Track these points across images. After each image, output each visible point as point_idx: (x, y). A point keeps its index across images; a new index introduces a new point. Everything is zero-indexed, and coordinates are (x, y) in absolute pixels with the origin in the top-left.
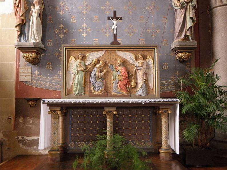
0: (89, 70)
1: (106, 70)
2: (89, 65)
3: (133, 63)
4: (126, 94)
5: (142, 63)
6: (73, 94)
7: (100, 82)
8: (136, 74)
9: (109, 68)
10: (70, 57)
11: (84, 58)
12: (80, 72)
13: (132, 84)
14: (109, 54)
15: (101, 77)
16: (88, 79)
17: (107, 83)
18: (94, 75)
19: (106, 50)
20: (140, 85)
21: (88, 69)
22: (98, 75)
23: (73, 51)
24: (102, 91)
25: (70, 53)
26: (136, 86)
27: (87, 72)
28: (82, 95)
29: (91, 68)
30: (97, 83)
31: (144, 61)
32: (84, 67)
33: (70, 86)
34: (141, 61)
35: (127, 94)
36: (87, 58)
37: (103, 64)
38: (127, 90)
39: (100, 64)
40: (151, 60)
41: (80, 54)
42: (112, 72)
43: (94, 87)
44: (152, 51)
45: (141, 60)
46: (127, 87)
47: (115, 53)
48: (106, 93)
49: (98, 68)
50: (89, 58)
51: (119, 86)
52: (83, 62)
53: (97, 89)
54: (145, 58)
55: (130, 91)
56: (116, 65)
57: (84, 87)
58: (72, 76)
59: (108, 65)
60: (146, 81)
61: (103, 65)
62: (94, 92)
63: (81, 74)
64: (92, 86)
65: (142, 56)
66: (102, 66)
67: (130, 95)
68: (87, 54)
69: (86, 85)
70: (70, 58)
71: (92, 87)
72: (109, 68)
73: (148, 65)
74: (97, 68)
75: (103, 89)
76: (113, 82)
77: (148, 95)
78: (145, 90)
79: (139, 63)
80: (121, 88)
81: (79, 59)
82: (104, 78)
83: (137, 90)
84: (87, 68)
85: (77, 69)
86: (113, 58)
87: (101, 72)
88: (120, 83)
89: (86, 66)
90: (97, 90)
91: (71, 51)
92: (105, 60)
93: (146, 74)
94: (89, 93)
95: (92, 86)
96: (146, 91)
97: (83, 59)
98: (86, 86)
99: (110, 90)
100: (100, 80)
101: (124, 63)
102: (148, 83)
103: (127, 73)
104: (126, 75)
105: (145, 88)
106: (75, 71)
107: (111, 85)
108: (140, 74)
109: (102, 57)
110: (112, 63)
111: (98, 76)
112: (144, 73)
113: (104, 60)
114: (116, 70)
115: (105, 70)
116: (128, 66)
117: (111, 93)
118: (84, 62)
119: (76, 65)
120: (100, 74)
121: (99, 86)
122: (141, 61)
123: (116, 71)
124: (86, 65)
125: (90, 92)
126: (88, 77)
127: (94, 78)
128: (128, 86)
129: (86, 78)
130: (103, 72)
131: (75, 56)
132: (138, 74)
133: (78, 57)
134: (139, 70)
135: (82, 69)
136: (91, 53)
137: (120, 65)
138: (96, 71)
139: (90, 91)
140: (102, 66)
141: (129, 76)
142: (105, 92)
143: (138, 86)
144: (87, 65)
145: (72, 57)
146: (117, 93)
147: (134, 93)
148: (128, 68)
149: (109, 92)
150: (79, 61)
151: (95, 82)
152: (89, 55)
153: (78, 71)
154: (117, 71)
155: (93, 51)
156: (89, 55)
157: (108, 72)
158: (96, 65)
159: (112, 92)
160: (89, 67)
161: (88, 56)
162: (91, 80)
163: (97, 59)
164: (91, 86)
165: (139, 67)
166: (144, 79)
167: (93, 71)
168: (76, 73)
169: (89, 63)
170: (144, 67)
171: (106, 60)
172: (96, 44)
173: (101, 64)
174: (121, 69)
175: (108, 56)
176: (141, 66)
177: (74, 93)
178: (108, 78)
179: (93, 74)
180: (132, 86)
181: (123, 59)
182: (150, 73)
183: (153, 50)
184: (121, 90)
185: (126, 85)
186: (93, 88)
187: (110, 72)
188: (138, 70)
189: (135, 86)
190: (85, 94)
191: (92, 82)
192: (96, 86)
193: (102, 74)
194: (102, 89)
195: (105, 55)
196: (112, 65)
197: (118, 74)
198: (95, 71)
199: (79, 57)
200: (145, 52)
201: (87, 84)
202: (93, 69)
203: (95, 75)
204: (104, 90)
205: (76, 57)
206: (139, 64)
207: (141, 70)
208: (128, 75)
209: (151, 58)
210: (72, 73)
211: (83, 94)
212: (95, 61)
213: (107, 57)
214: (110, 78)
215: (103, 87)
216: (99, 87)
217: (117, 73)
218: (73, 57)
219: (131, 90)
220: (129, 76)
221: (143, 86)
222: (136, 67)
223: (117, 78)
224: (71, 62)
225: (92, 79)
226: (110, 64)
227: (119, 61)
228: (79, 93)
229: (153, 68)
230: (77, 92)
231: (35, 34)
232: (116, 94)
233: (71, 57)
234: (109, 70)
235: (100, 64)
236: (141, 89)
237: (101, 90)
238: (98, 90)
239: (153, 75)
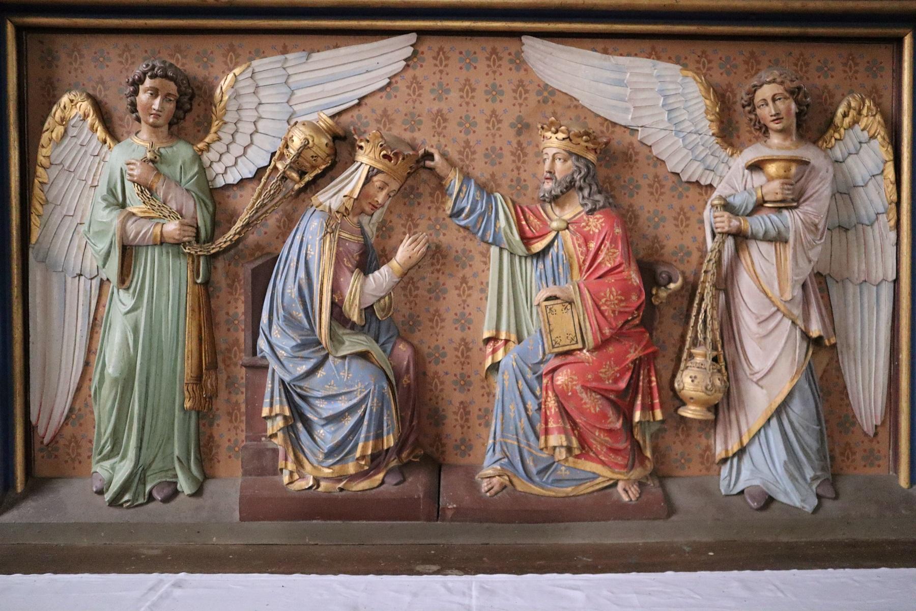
0: (252, 238)
1: (423, 237)
2: (243, 182)
3: (694, 172)
4: (626, 493)
5: (794, 169)
6: (91, 475)
7: (358, 364)
8: (726, 284)
9: (456, 214)
10: (52, 100)
11: (190, 111)
12: (150, 263)
13: (689, 382)
14: (455, 74)
15: (369, 311)
16: (242, 336)
17: (432, 368)
18: (292, 291)
19: (422, 33)
20: (759, 400)
21: (239, 224)
22: (336, 289)
23: (79, 39)
24: (377, 460)
25: (50, 60)
26: (723, 405)
27: (228, 261)
28: (176, 493)
29: (272, 221)
30: (321, 373)
31: (808, 153)
32: (189, 206)
33: (62, 404)
34: (777, 145)
35: (634, 491)
36: (230, 117)
37: (391, 173)
38: (637, 448)
39: (363, 172)
40: (875, 143)
41: (143, 67)
42: (486, 255)
43: (298, 417)
44: (883, 54)
45: (775, 139)
46: (637, 416)
47: (519, 62)
48: (417, 485)
49: (334, 222)
50: (249, 115)
51: (552, 403)
52: (182, 151)
53: (327, 436)
54: (813, 122)
55: (655, 450)
56: (519, 185)
57: (204, 412)
58: (77, 300)
59: (440, 186)
60: (823, 363)
61: (395, 186)
62: (298, 462)
63: (168, 280)
64: (274, 408)
65: (794, 93)
66: (381, 197)
67: (667, 498)
68: (225, 73)
69: (223, 394)
70: (57, 112)
71: (280, 422)
72: (456, 214)
73: (844, 192)
74: (330, 215)
75: (390, 441)
76: (495, 366)
77: (836, 498)
78: (812, 442)
79: (756, 167)
80: (574, 425)
81: (145, 132)
82: (399, 319)
83: (734, 447)
84: (232, 218)
85: (116, 223)
86: (494, 118)
87: (368, 261)
88: (561, 378)
89: (215, 197)
90: (326, 447)
91: (62, 39)
92: (407, 136)
93: (821, 286)
94: (246, 473)
95: (274, 408)
96: (823, 458)
97: (188, 123)
98: (220, 403)
99: (465, 446)
100: (353, 343)
101: (608, 164)
102: (839, 369)
103: (635, 279)
104: (626, 290)
105: (807, 429)
106: (103, 246)
107: (476, 391)
108: (765, 284)
109: (378, 102)
110: (481, 169)
111: (337, 309)
112: (806, 269)
113: (398, 130)
114: (526, 240)
115: (407, 242)
116: (644, 204)
117: (471, 471)
118: (198, 157)
119: (111, 192)
120: (352, 284)
121: (351, 410)
122: (777, 145)
123: (521, 249)
124: (220, 182)
125: (262, 463)
126: (240, 308)
127: (290, 320)
128: (648, 407)
129: (221, 317)
130: (385, 257)
131: (100, 96)
132: (745, 283)
133: (133, 107)
134: (766, 238)
135: (172, 227)
136: (267, 66)
137: (570, 186)
138: (314, 254)
139: (260, 453)
140: (381, 197)
141: (658, 308)
142: (404, 469)
143: (741, 402)
144: (228, 186)
145: (73, 106)
146: (530, 479)
147: (695, 469)
148: (644, 216)
149: (452, 458)
150: (139, 144)
151: (303, 368)
152: (246, 86)
153: (128, 253)
154: (538, 246)
155: (288, 40)
156: (246, 86)
157: (436, 255)
158: (314, 185)
159: (480, 467)
160: (246, 204)
161: (237, 96)
162: (262, 343)
163: (323, 119)
164: (265, 412)
165: (760, 205)
166: (805, 335)
167: (289, 252)
168: (112, 270)
169: (248, 171)
170: (816, 207)
171: (419, 136)
172: (41, 159)
173: (368, 179)
174: (572, 224)
175: (442, 92)
176: (783, 205)
177: (101, 469)
178: (436, 317)
179: (284, 286)
180: (683, 403)
181: (594, 126)
182: (857, 267)
183: (900, 41)
184: (569, 449)
185: (622, 404)
186: (289, 429)
187: (463, 259)
188: (741, 238)
189: (715, 409)
190: (211, 486)
191: (273, 364)
192: (322, 405)
193: (383, 277)
194: (379, 437)
195: (416, 85)
196: (481, 187)
197: (543, 277)
198: (311, 247)
199: (143, 97)
200: (814, 63)
201: (231, 383)
202: (289, 223)
203: (305, 297)
204: (401, 445)
205: (118, 106)
206: (758, 179)
207: (778, 239)
208: (649, 295)
209: (873, 122)
210: (74, 264)
211: (185, 486)
212: (305, 146)
213: (428, 104)
214: (465, 322)
215: (390, 420)
216: (350, 422)
217: (532, 270)
218: (85, 106)
219: (675, 446)
220: (658, 308)
221: (796, 407)
222: (727, 207)
223: (532, 325)
224: (67, 153)
225: (278, 339)
226: (467, 177)
227: (553, 143)
228: (143, 481)
229: (886, 223)
230: (123, 469)
231: (859, 330)
232: (522, 485)
233: (65, 99)
234: (451, 238)
235: (351, 183)
236: (774, 433)
237: (364, 446)
238: (339, 450)
239: (886, 292)
